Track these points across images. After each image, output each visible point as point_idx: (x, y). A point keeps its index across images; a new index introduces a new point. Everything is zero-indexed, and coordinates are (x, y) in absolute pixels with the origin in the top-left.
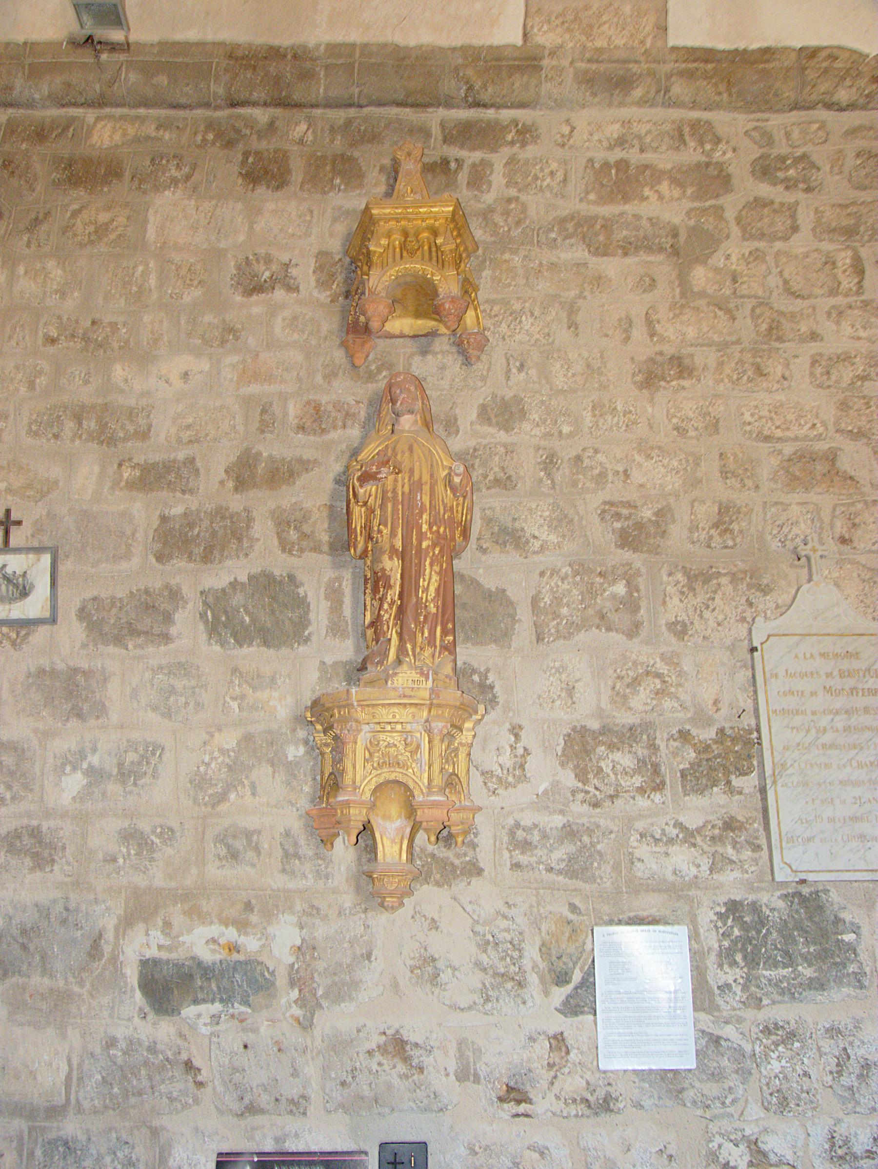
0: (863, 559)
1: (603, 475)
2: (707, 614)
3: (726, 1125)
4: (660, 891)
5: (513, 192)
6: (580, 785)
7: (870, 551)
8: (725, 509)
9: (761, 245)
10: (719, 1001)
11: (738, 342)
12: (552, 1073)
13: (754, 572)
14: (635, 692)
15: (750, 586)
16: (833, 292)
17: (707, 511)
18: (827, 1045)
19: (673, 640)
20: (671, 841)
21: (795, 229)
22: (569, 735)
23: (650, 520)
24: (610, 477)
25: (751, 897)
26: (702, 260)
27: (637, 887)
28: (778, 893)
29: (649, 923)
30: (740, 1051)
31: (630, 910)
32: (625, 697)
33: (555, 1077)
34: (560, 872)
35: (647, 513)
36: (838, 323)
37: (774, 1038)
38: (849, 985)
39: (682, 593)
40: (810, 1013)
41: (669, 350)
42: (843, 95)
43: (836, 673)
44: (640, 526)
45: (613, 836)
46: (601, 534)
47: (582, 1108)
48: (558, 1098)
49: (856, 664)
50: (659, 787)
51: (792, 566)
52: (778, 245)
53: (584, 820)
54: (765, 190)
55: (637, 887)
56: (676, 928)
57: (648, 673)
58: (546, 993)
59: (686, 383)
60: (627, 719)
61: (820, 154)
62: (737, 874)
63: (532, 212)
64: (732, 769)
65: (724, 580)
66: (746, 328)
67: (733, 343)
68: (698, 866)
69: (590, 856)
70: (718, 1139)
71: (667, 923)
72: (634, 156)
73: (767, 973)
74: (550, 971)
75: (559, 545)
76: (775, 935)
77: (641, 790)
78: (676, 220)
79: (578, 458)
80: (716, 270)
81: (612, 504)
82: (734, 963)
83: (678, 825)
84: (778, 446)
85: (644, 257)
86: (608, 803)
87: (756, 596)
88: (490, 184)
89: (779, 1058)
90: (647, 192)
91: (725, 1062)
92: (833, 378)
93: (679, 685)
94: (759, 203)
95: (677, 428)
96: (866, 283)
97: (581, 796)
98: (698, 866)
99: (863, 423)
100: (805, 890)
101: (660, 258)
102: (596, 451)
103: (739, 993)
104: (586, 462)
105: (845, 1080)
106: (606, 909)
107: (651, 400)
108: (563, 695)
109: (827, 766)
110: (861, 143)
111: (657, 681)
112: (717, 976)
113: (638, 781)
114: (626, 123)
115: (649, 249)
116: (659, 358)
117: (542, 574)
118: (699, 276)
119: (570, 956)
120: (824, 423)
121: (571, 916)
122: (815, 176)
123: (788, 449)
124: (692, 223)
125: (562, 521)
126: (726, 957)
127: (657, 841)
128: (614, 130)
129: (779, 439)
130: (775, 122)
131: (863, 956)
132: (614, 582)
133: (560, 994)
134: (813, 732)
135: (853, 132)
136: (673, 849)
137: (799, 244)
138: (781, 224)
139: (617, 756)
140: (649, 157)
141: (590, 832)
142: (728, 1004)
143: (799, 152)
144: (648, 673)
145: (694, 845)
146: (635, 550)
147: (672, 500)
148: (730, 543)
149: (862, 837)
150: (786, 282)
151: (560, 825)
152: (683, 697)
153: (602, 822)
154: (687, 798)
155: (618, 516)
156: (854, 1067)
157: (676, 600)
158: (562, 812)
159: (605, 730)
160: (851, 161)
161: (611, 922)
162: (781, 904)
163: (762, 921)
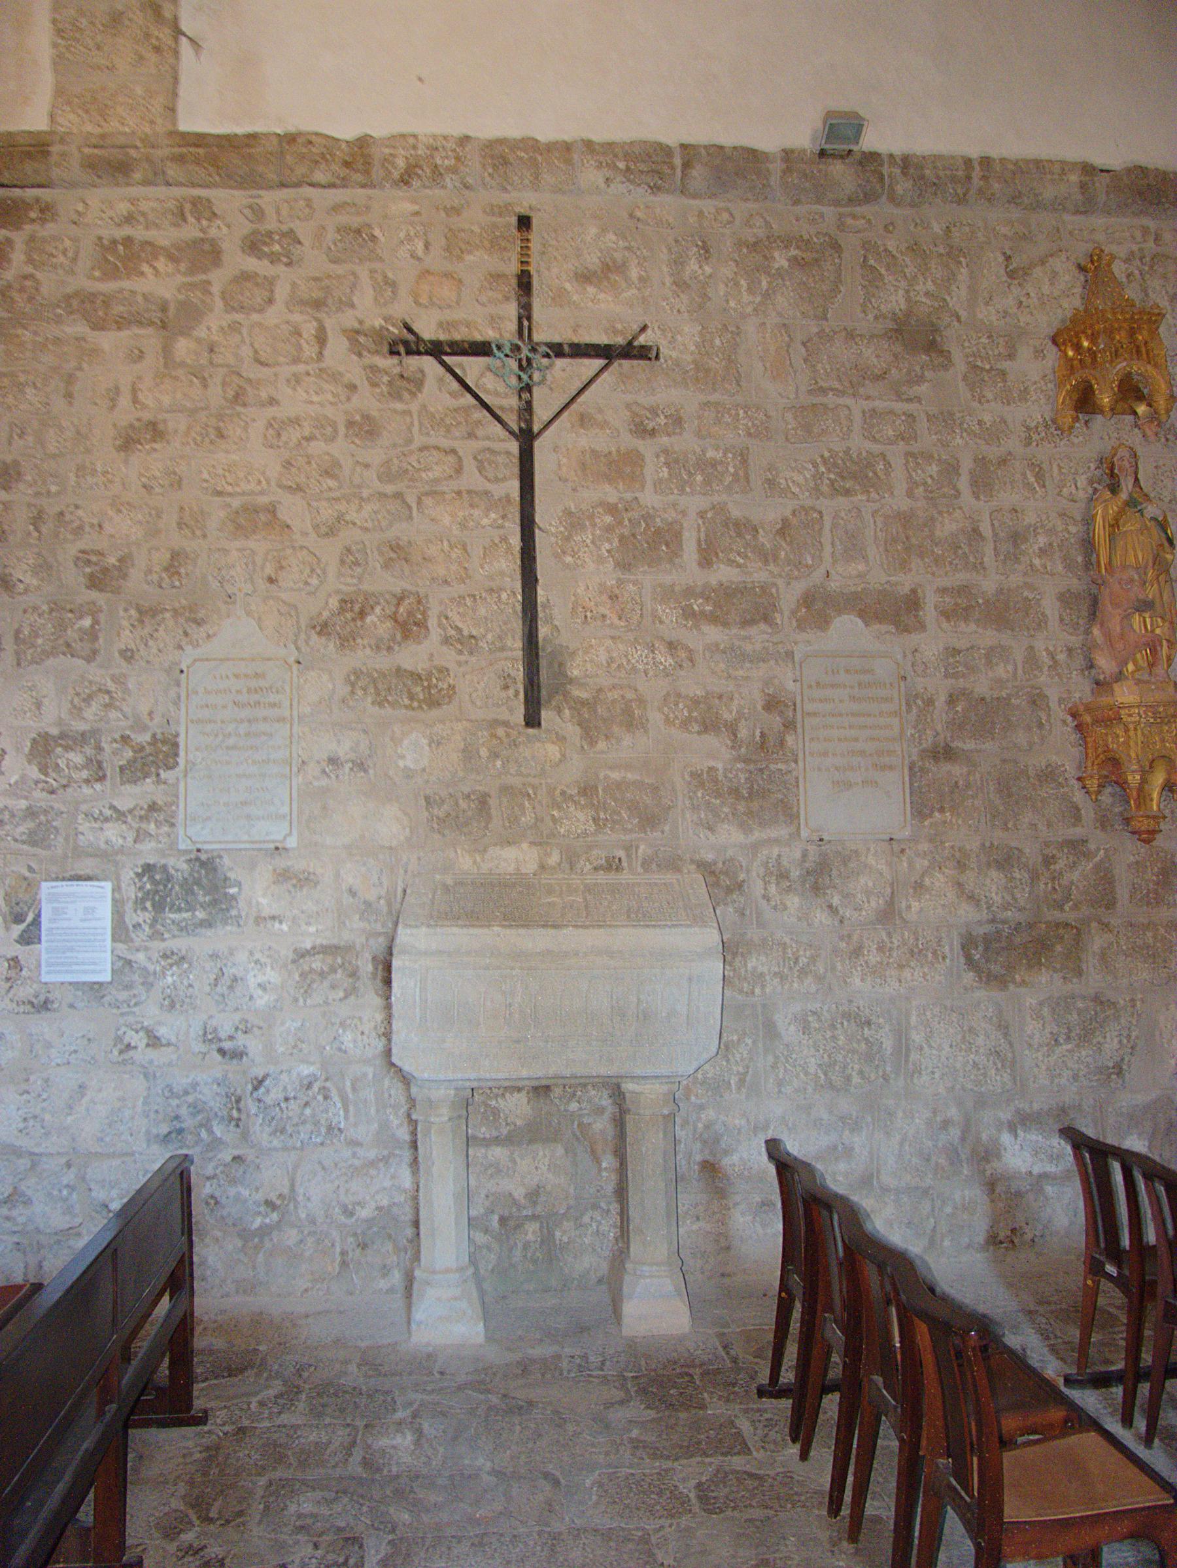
0: (283, 595)
1: (81, 528)
2: (151, 643)
3: (131, 1019)
4: (96, 856)
5: (30, 269)
6: (43, 777)
7: (292, 589)
8: (175, 555)
9: (238, 317)
10: (133, 936)
11: (207, 408)
12: (9, 984)
13: (192, 608)
14: (89, 705)
15: (188, 620)
16: (296, 361)
17: (162, 557)
18: (209, 965)
19: (124, 664)
20: (107, 820)
21: (271, 301)
22: (34, 740)
23: (114, 566)
24: (87, 529)
25: (163, 862)
26: (185, 332)
27: (79, 853)
28: (183, 859)
29: (85, 880)
30: (145, 969)
31: (73, 869)
32: (80, 709)
33: (11, 987)
34: (24, 842)
35: (112, 560)
36: (294, 389)
37: (169, 961)
38: (232, 925)
39: (133, 625)
40: (200, 944)
41: (147, 416)
42: (319, 176)
43: (245, 690)
44: (105, 571)
45: (64, 815)
46: (74, 577)
47: (28, 1008)
48: (12, 1001)
49: (262, 683)
50: (101, 779)
51: (226, 603)
52: (255, 317)
53: (43, 804)
54: (252, 264)
55: (79, 853)
56: (103, 884)
57: (100, 690)
58: (7, 929)
59: (157, 446)
60: (81, 726)
61: (304, 230)
62: (153, 844)
63: (44, 290)
64: (161, 764)
65: (168, 615)
66: (216, 395)
67: (202, 409)
68: (125, 838)
69: (48, 830)
70: (123, 1029)
71: (98, 880)
72: (139, 233)
73: (171, 916)
74: (11, 913)
75: (38, 588)
76: (177, 888)
77: (87, 781)
78: (168, 296)
79: (62, 514)
80: (199, 341)
81: (83, 552)
82: (145, 909)
83: (113, 807)
84: (228, 500)
85: (136, 330)
86: (61, 791)
87: (192, 629)
88: (9, 261)
89: (173, 975)
90: (145, 268)
91: (136, 977)
92: (284, 438)
93: (124, 700)
94: (245, 277)
95: (145, 486)
96: (326, 353)
97: (40, 786)
98: (125, 838)
99: (302, 479)
100: (203, 857)
101: (150, 331)
102: (77, 507)
103: (147, 929)
104: (68, 517)
105: (219, 989)
106: (54, 869)
107: (126, 462)
108: (33, 708)
109: (228, 763)
110: (343, 219)
111: (106, 697)
112: (131, 918)
113: (85, 774)
114: (133, 201)
115: (140, 323)
116: (137, 424)
117: (25, 611)
118: (183, 347)
119: (26, 903)
120: (268, 482)
121: (27, 874)
122: (296, 251)
123: (236, 503)
124: (181, 297)
125: (44, 568)
126: (140, 904)
127: (96, 820)
128: (123, 208)
129: (230, 494)
130: (268, 198)
131: (241, 904)
132: (81, 617)
133: (18, 929)
134: (221, 737)
135: (336, 208)
136: (106, 825)
137: (274, 316)
138: (259, 296)
139: (71, 755)
140: (152, 235)
141: (46, 812)
142: (139, 938)
143: (284, 228)
144: (100, 690)
145: (125, 822)
146: (101, 590)
147: (134, 548)
148: (177, 583)
149: (248, 817)
150: (256, 352)
151: (24, 807)
152: (125, 709)
153: (56, 805)
154: (123, 788)
155: (89, 562)
156: (226, 981)
157: (127, 632)
158: (26, 798)
159: (63, 736)
160: (331, 235)
161: (57, 879)
162: (185, 866)
163: (169, 878)
